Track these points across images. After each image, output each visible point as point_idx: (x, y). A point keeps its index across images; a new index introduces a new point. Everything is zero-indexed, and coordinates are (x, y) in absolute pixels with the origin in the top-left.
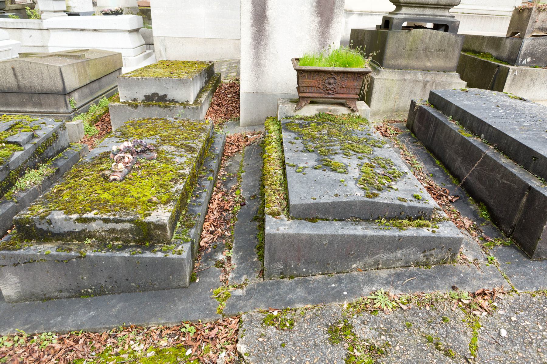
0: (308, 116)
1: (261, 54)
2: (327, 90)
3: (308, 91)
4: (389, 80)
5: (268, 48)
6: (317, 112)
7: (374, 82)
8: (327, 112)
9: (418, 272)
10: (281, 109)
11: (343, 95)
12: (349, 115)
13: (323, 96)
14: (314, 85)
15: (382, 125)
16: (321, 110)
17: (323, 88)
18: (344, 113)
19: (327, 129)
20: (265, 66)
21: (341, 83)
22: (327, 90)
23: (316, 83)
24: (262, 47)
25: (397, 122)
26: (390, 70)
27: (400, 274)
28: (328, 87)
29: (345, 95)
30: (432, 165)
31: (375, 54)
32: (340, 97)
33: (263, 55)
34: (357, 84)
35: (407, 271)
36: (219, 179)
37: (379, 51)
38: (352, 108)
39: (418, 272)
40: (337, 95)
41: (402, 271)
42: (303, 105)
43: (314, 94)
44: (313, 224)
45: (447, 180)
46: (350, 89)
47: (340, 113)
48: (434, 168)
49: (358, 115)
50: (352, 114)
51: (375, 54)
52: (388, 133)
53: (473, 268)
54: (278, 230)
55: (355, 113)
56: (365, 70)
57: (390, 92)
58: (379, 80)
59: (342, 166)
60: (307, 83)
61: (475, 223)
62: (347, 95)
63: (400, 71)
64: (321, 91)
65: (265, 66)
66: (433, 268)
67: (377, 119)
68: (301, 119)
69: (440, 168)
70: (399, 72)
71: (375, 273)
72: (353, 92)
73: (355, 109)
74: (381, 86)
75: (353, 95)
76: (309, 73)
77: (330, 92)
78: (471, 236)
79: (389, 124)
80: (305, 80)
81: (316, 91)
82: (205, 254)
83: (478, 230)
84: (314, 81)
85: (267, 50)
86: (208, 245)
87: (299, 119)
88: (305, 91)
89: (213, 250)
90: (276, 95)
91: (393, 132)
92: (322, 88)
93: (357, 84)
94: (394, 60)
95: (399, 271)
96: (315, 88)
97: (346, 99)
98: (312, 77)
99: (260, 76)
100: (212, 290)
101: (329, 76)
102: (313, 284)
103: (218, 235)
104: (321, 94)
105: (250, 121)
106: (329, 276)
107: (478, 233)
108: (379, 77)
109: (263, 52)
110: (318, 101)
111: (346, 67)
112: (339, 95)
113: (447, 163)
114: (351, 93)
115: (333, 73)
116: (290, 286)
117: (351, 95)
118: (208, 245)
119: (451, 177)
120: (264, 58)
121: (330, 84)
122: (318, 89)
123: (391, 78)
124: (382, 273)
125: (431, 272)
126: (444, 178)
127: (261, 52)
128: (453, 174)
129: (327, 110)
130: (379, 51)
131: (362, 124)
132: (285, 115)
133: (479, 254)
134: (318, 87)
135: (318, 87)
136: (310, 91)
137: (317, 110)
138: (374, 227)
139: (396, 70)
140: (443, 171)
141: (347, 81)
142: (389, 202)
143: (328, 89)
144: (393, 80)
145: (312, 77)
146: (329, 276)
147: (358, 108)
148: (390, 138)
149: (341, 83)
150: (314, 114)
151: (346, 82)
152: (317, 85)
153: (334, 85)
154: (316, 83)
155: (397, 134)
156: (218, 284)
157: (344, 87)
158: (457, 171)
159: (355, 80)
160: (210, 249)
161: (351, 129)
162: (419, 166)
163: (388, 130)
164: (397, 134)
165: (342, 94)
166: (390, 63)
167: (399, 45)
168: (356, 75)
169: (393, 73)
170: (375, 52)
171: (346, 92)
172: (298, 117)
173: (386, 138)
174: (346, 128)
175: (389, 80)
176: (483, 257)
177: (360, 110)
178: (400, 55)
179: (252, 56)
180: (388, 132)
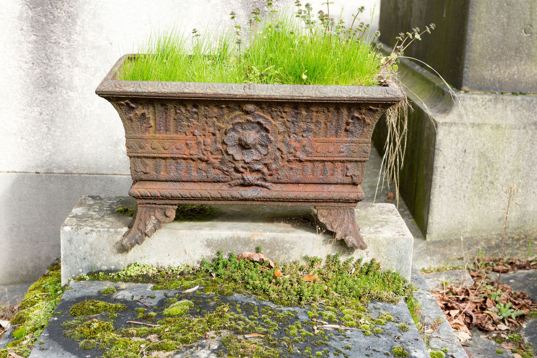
0: (175, 266)
1: (56, 49)
2: (237, 170)
3: (163, 175)
4: (487, 129)
5: (78, 28)
6: (209, 254)
7: (435, 134)
8: (247, 254)
10: (70, 241)
11: (301, 187)
12: (332, 260)
13: (225, 194)
14: (186, 152)
15: (469, 283)
16: (224, 243)
17: (222, 162)
18: (311, 255)
19: (225, 333)
20: (71, 88)
21: (288, 145)
22: (237, 170)
23: (192, 143)
24: (57, 28)
25: (521, 267)
26: (487, 97)
28: (238, 157)
29: (309, 188)
31: (418, 36)
32: (291, 195)
33: (64, 53)
34: (353, 147)
37: (432, 26)
38: (338, 237)
40: (278, 187)
42: (150, 227)
43: (188, 186)
46: (329, 165)
47: (295, 255)
49: (366, 260)
50: (342, 259)
51: (418, 36)
52: (491, 318)
55: (357, 255)
56: (378, 93)
57: (490, 165)
58: (454, 129)
59: (455, 239)
60: (156, 144)
62: (319, 187)
63: (519, 98)
64: (214, 173)
65: (71, 88)
67: (455, 255)
68: (145, 279)
70: (516, 102)
72: (339, 177)
73: (351, 240)
74: (460, 146)
75: (340, 188)
76: (159, 108)
77: (250, 177)
79: (493, 276)
80: (147, 135)
81: (195, 175)
84: (182, 136)
85: (75, 37)
87: (135, 279)
88: (153, 174)
90: (112, 181)
91: (506, 313)
92: (217, 163)
93: (353, 147)
94: (498, 66)
96: (193, 164)
97: (316, 201)
98: (172, 123)
99: (57, 119)
101: (238, 117)
104: (218, 186)
105: (30, 265)
108: (450, 118)
109: (63, 42)
110: (224, 209)
111: (301, 81)
112: (285, 188)
114: (333, 179)
115: (250, 107)
117: (332, 188)
120: (65, 61)
121: (244, 146)
122: (203, 165)
123: (492, 120)
127: (57, 43)
129: (246, 242)
130: (432, 26)
131: (380, 299)
132: (85, 264)
134: (202, 160)
135: (202, 160)
136: (173, 175)
137: (209, 244)
139: (508, 97)
141: (310, 136)
143: (239, 165)
144: (498, 126)
145: (172, 123)
147: (366, 233)
148: (499, 340)
149: (288, 145)
150: (198, 258)
151: (308, 139)
152: (195, 152)
153: (263, 151)
154: (192, 143)
155: (522, 317)
157: (303, 157)
159: (342, 133)
161: (329, 327)
163: (489, 303)
164: (522, 317)
165: (298, 183)
166: (487, 74)
167: (509, 18)
168: (345, 112)
169: (499, 106)
170: (416, 30)
171: (310, 177)
172: (133, 272)
173: (483, 337)
174: (308, 325)
175: (487, 129)
177: (374, 241)
178: (517, 50)
179: (29, 57)
180: (491, 310)
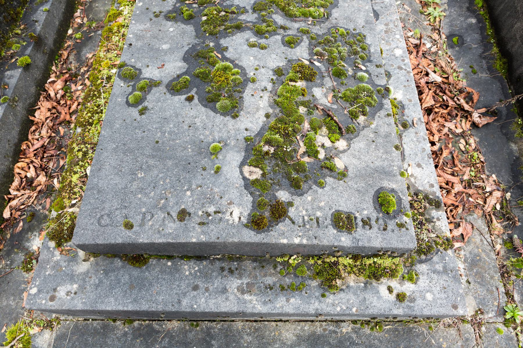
9: (354, 336)
27: (319, 337)
30: (464, 9)
35: (335, 332)
36: (70, 37)
39: (354, 336)
41: (325, 330)
44: (136, 272)
45: (484, 58)
48: (467, 18)
53: (467, 340)
54: (52, 299)
61: (508, 195)
66: (388, 331)
69: (479, 21)
71: (274, 330)
78: (487, 236)
82: (12, 235)
83: (509, 219)
86: (20, 213)
89: (26, 226)
95: (319, 330)
100: (5, 328)
102: (161, 342)
103: (39, 188)
106: (192, 325)
107: (505, 227)
113: (497, 12)
116: (123, 339)
118: (20, 213)
119: (495, 49)
124: (288, 330)
125: (381, 342)
126: (480, 51)
128: (501, 44)
133: (492, 292)
138: (270, 280)
140: (482, 29)
142: (305, 242)
146: (192, 325)
156: (18, 314)
158: (512, 43)
160: (21, 224)
162: (436, 14)
176: (496, 304)
